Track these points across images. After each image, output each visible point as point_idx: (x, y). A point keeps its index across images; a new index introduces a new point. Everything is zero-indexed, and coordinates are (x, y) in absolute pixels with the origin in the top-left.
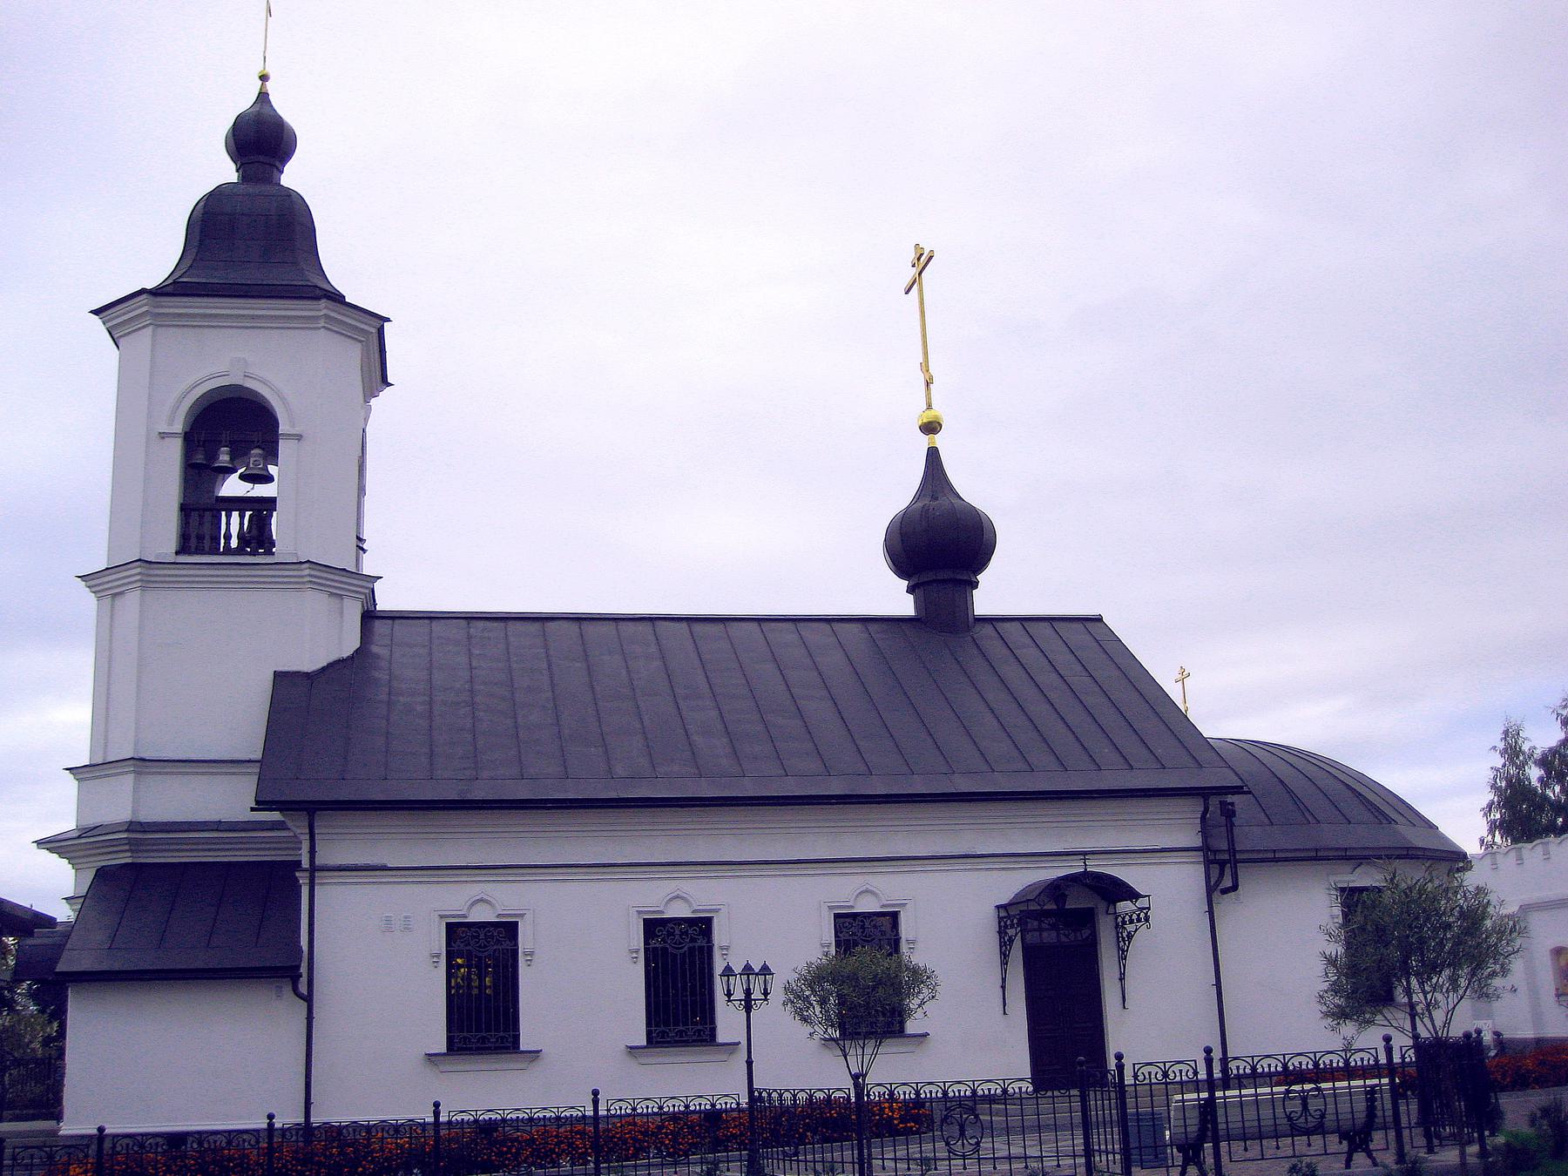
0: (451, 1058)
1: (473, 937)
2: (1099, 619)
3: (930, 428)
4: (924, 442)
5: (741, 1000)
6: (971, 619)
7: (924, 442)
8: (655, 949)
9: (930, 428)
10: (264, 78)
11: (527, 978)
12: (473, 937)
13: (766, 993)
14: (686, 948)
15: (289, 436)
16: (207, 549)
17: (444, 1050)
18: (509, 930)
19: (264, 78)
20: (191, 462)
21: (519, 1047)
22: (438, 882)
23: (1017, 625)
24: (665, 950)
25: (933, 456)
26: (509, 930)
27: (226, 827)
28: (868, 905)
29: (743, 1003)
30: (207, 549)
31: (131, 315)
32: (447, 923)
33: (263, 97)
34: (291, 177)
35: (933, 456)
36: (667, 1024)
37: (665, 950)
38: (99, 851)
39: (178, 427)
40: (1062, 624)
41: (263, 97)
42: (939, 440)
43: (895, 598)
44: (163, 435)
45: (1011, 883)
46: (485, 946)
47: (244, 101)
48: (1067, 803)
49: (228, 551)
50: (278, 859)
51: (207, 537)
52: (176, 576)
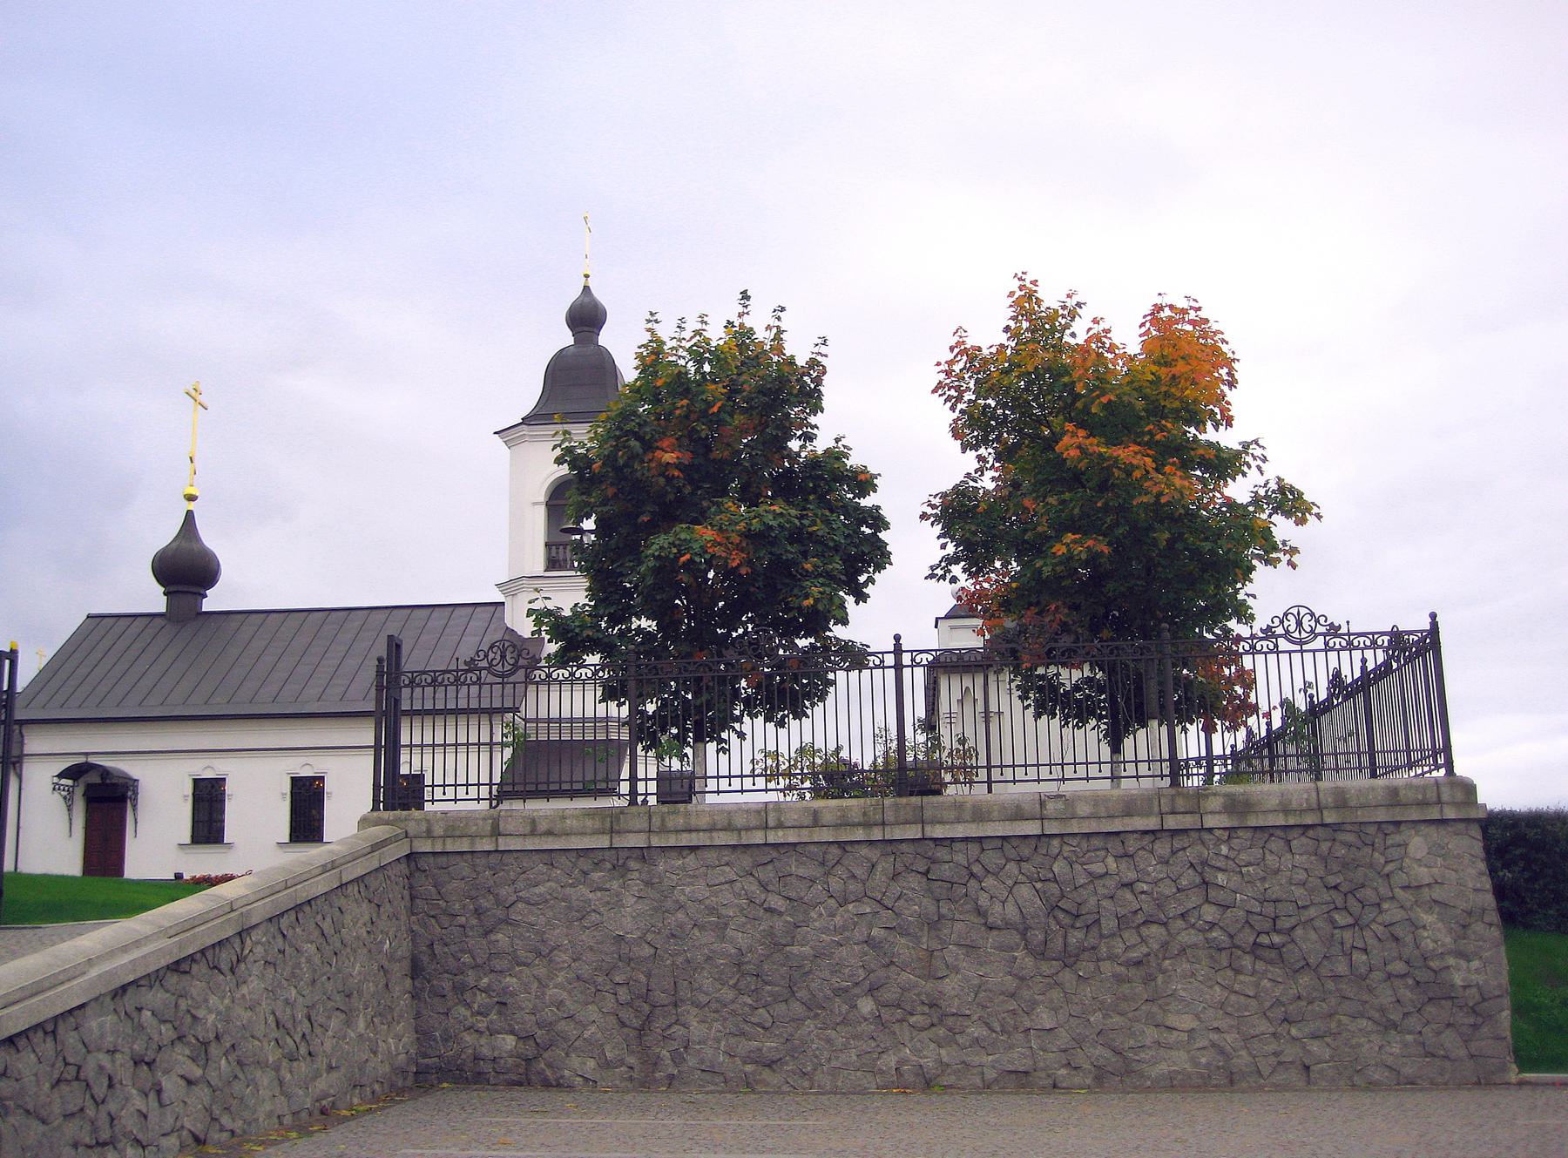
19: (587, 276)
28: (306, 772)
33: (586, 289)
39: (542, 498)
41: (586, 289)
44: (535, 504)
47: (575, 293)
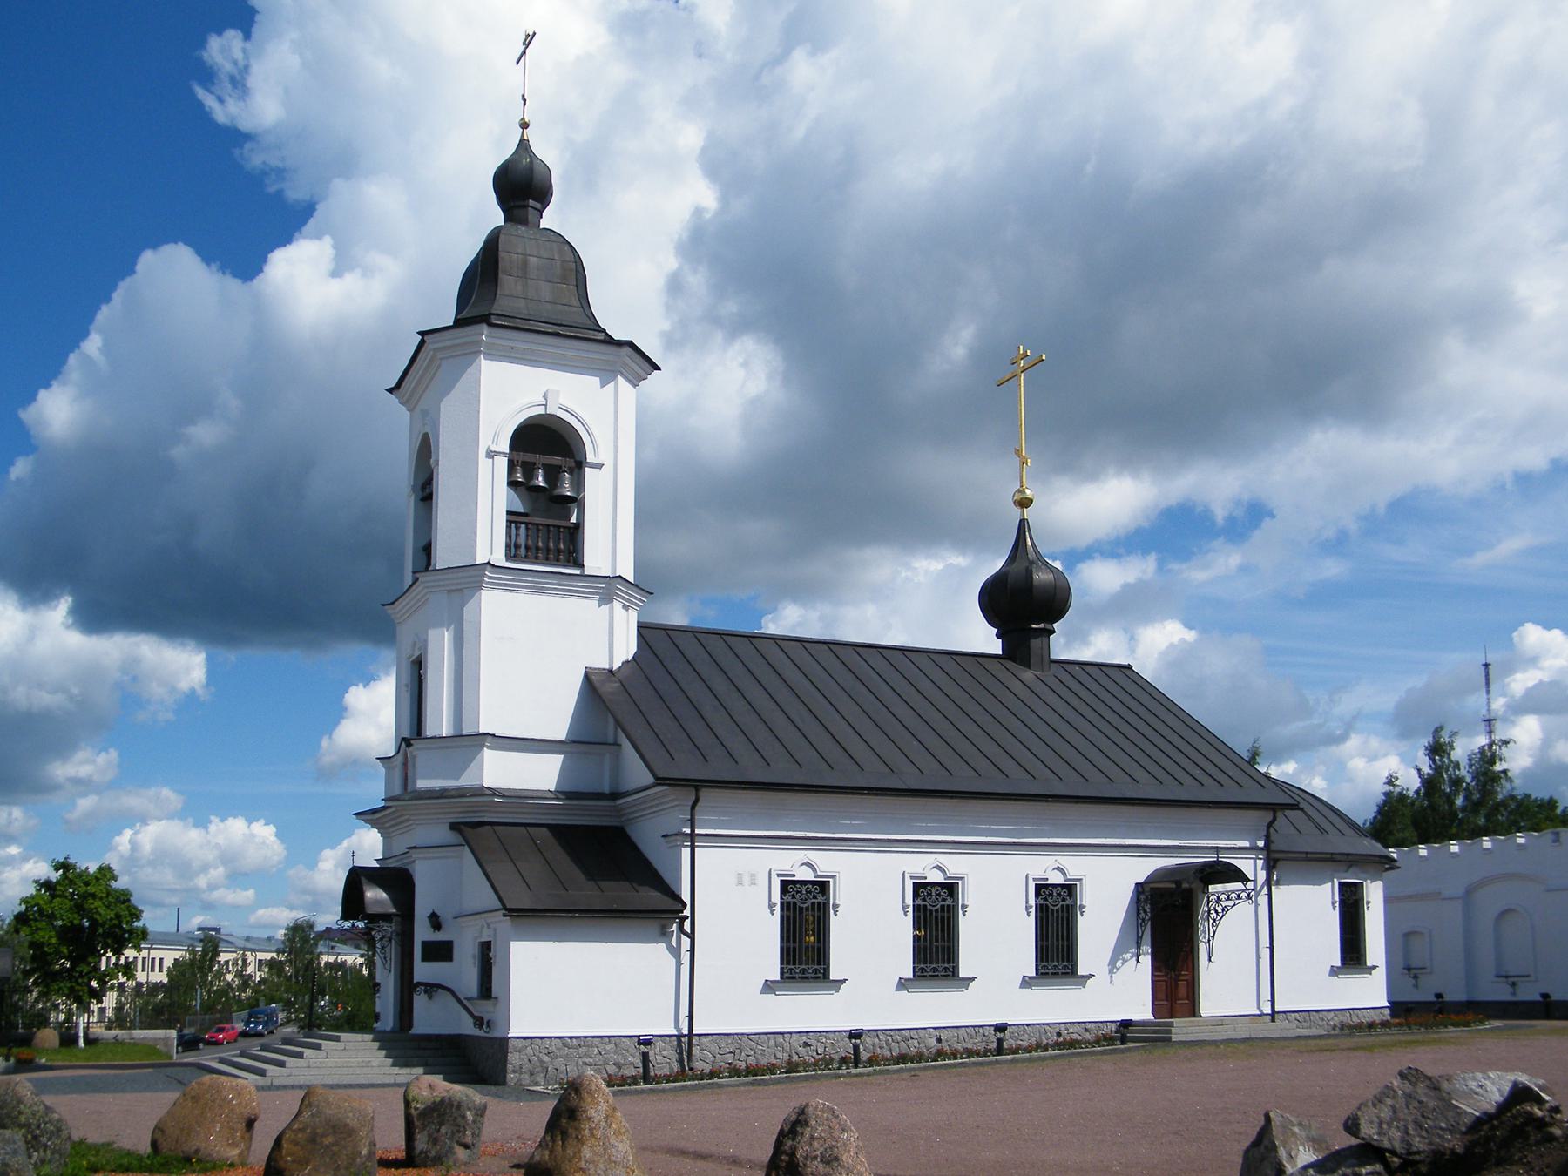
0: (917, 983)
1: (798, 892)
3: (1024, 503)
6: (1045, 659)
8: (919, 906)
11: (835, 923)
12: (798, 892)
14: (1059, 906)
17: (778, 978)
18: (822, 886)
20: (513, 479)
21: (829, 978)
22: (950, 853)
23: (1095, 668)
24: (925, 906)
25: (1023, 525)
26: (822, 886)
27: (438, 795)
32: (914, 883)
33: (524, 145)
35: (1023, 525)
36: (925, 963)
37: (925, 906)
38: (536, 811)
41: (524, 145)
42: (1028, 513)
43: (984, 639)
45: (1142, 868)
46: (806, 900)
48: (1137, 808)
50: (591, 823)
51: (523, 546)
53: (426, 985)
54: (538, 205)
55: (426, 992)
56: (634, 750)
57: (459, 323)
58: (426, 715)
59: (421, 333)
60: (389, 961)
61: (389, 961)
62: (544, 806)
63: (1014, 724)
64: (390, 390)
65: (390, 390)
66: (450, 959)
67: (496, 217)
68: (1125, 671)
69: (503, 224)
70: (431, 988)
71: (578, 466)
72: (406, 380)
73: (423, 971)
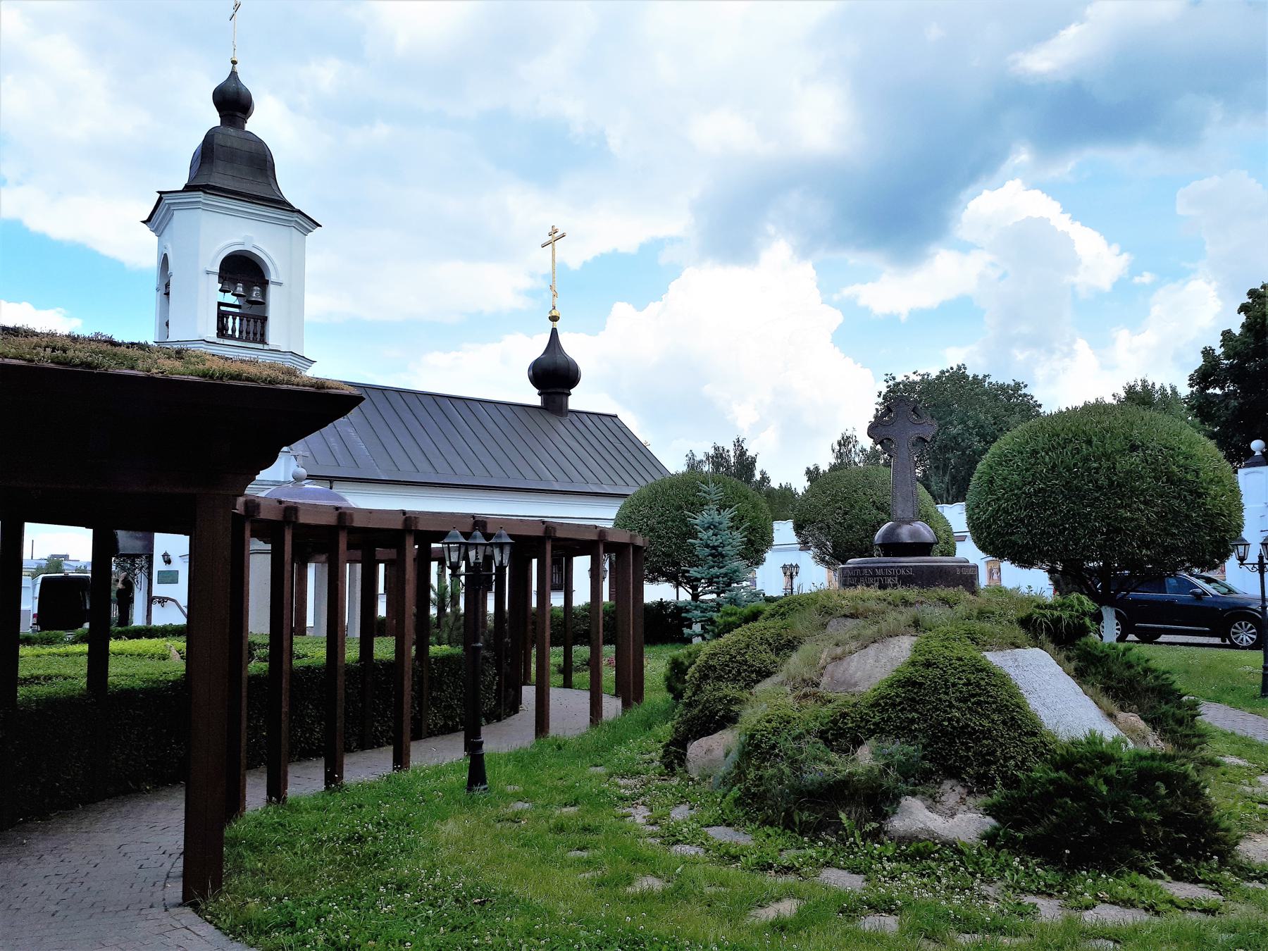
2: (616, 416)
3: (554, 319)
4: (550, 325)
5: (1254, 564)
7: (550, 325)
9: (554, 319)
10: (234, 63)
13: (797, 573)
15: (274, 283)
16: (258, 340)
19: (234, 63)
25: (554, 333)
29: (1257, 566)
30: (258, 340)
31: (306, 226)
33: (233, 74)
34: (252, 125)
35: (554, 333)
40: (603, 417)
41: (233, 74)
42: (557, 325)
43: (532, 397)
47: (222, 77)
49: (232, 337)
52: (299, 362)
53: (159, 598)
54: (243, 116)
55: (159, 602)
56: (570, 536)
57: (188, 188)
58: (143, 601)
59: (160, 193)
60: (140, 583)
61: (140, 583)
62: (351, 588)
63: (627, 455)
64: (144, 222)
65: (144, 222)
66: (177, 583)
67: (214, 119)
68: (613, 418)
69: (219, 125)
70: (163, 600)
71: (264, 284)
72: (153, 218)
73: (158, 590)
